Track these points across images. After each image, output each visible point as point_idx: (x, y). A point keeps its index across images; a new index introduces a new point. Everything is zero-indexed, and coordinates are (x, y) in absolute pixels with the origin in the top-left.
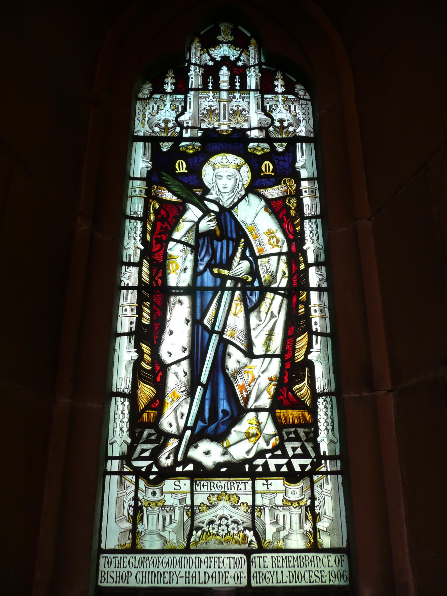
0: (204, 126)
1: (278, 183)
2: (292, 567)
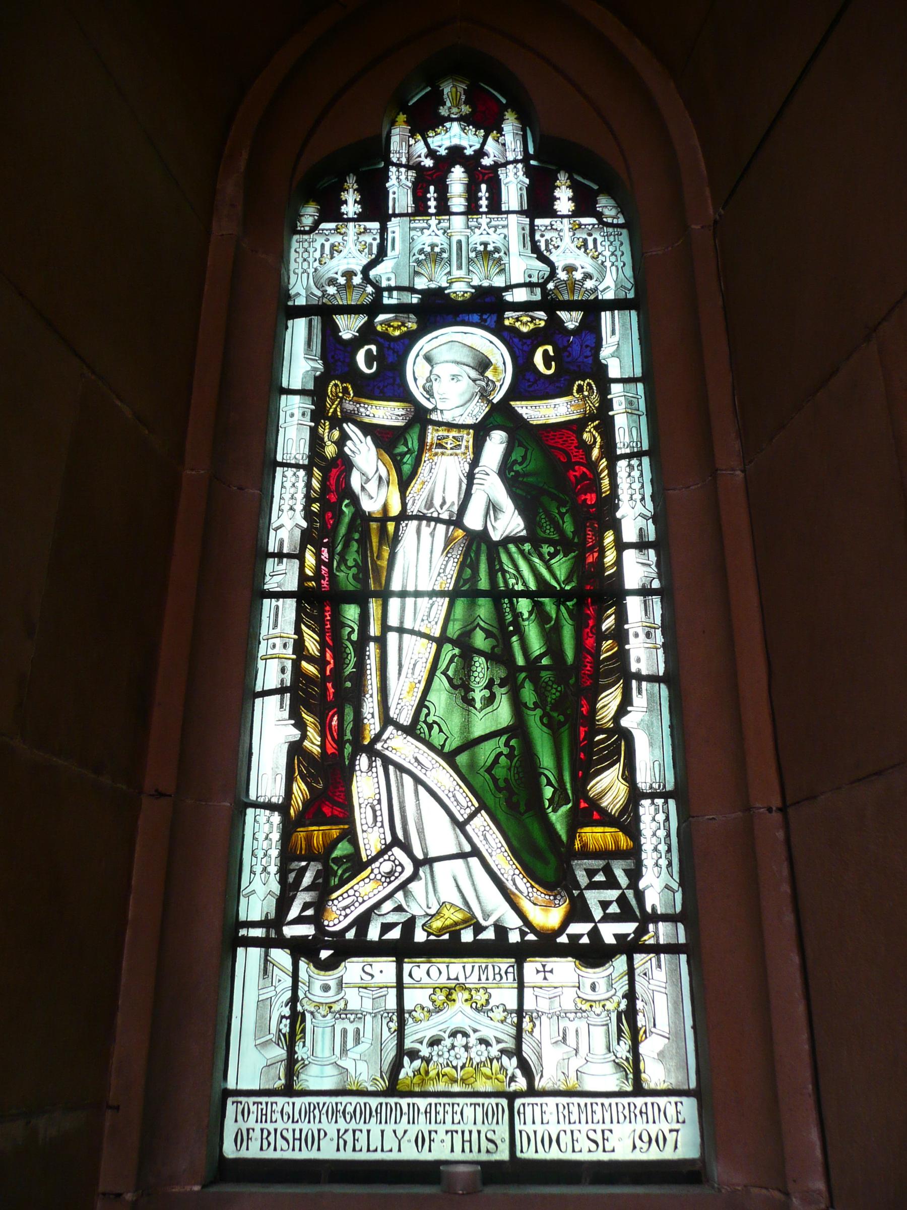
0: (421, 283)
1: (566, 392)
2: (598, 1122)
